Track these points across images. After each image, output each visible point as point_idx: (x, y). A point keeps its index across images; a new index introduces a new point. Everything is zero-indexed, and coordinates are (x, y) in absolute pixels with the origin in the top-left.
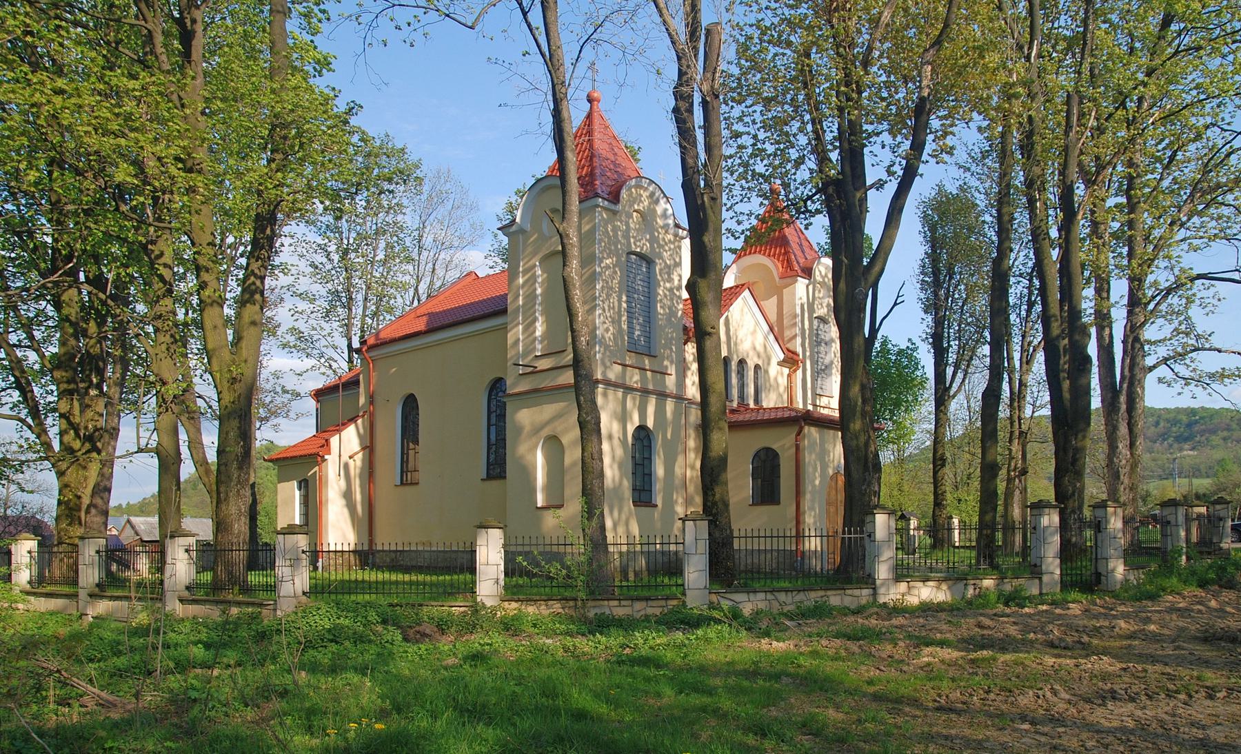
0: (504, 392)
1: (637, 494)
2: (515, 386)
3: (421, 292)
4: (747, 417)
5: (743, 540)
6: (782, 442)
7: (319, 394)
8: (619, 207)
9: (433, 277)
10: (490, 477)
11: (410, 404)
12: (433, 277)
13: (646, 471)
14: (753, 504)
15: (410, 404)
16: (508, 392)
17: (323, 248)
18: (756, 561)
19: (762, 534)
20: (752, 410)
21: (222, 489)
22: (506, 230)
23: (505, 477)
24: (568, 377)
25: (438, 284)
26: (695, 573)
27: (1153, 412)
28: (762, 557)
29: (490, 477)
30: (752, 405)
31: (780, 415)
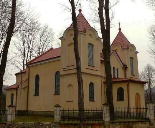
0: (59, 74)
1: (90, 98)
2: (62, 73)
3: (40, 52)
4: (116, 80)
5: (124, 110)
6: (124, 86)
7: (16, 75)
8: (86, 34)
9: (43, 49)
10: (55, 94)
11: (37, 77)
12: (43, 49)
13: (92, 93)
14: (117, 101)
15: (37, 77)
16: (60, 74)
17: (19, 43)
18: (121, 114)
19: (117, 108)
20: (117, 78)
21: (137, 99)
22: (61, 39)
23: (38, 95)
24: (75, 71)
25: (43, 51)
26: (106, 119)
27: (5, 86)
28: (122, 114)
29: (55, 94)
30: (116, 78)
31: (122, 80)
